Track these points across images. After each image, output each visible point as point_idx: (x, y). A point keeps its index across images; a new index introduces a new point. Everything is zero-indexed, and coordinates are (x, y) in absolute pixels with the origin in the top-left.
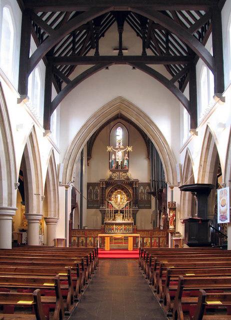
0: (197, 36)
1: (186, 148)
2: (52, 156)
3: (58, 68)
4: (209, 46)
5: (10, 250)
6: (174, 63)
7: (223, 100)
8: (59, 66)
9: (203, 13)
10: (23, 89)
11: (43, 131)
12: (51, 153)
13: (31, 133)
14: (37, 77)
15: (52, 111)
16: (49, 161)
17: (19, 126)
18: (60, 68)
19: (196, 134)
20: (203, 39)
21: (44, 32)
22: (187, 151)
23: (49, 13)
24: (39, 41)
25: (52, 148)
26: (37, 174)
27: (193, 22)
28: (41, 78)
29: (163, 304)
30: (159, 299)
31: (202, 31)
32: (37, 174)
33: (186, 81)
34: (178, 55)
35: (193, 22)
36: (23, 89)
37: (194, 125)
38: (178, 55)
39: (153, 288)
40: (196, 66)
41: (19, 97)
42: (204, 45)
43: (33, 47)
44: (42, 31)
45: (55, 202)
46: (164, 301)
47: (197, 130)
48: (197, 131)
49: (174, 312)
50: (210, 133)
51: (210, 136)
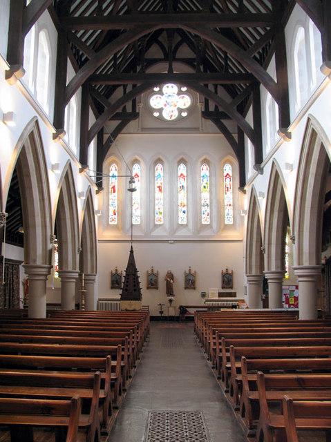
0: (258, 56)
1: (272, 159)
2: (69, 172)
3: (79, 35)
4: (272, 70)
5: (44, 320)
6: (238, 82)
7: (244, 192)
8: (82, 32)
9: (268, 28)
10: (59, 123)
11: (53, 131)
12: (67, 168)
13: (67, 172)
14: (73, 109)
15: (26, 29)
16: (63, 179)
17: (55, 167)
18: (99, 88)
19: (289, 136)
20: (264, 62)
21: (83, 54)
22: (252, 189)
23: (91, 31)
24: (79, 65)
25: (69, 160)
26: (42, 199)
27: (258, 38)
28: (51, 52)
29: (229, 394)
30: (225, 389)
31: (263, 52)
32: (42, 199)
33: (249, 102)
34: (244, 72)
35: (258, 38)
36: (59, 123)
37: (285, 122)
38: (244, 72)
39: (206, 355)
40: (285, 29)
41: (8, 69)
42: (266, 68)
43: (71, 73)
44: (81, 53)
45: (92, 260)
46: (241, 408)
47: (290, 129)
48: (289, 131)
49: (241, 405)
50: (277, 172)
51: (314, 134)
